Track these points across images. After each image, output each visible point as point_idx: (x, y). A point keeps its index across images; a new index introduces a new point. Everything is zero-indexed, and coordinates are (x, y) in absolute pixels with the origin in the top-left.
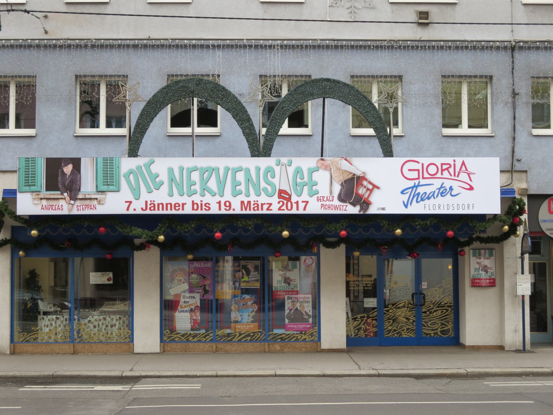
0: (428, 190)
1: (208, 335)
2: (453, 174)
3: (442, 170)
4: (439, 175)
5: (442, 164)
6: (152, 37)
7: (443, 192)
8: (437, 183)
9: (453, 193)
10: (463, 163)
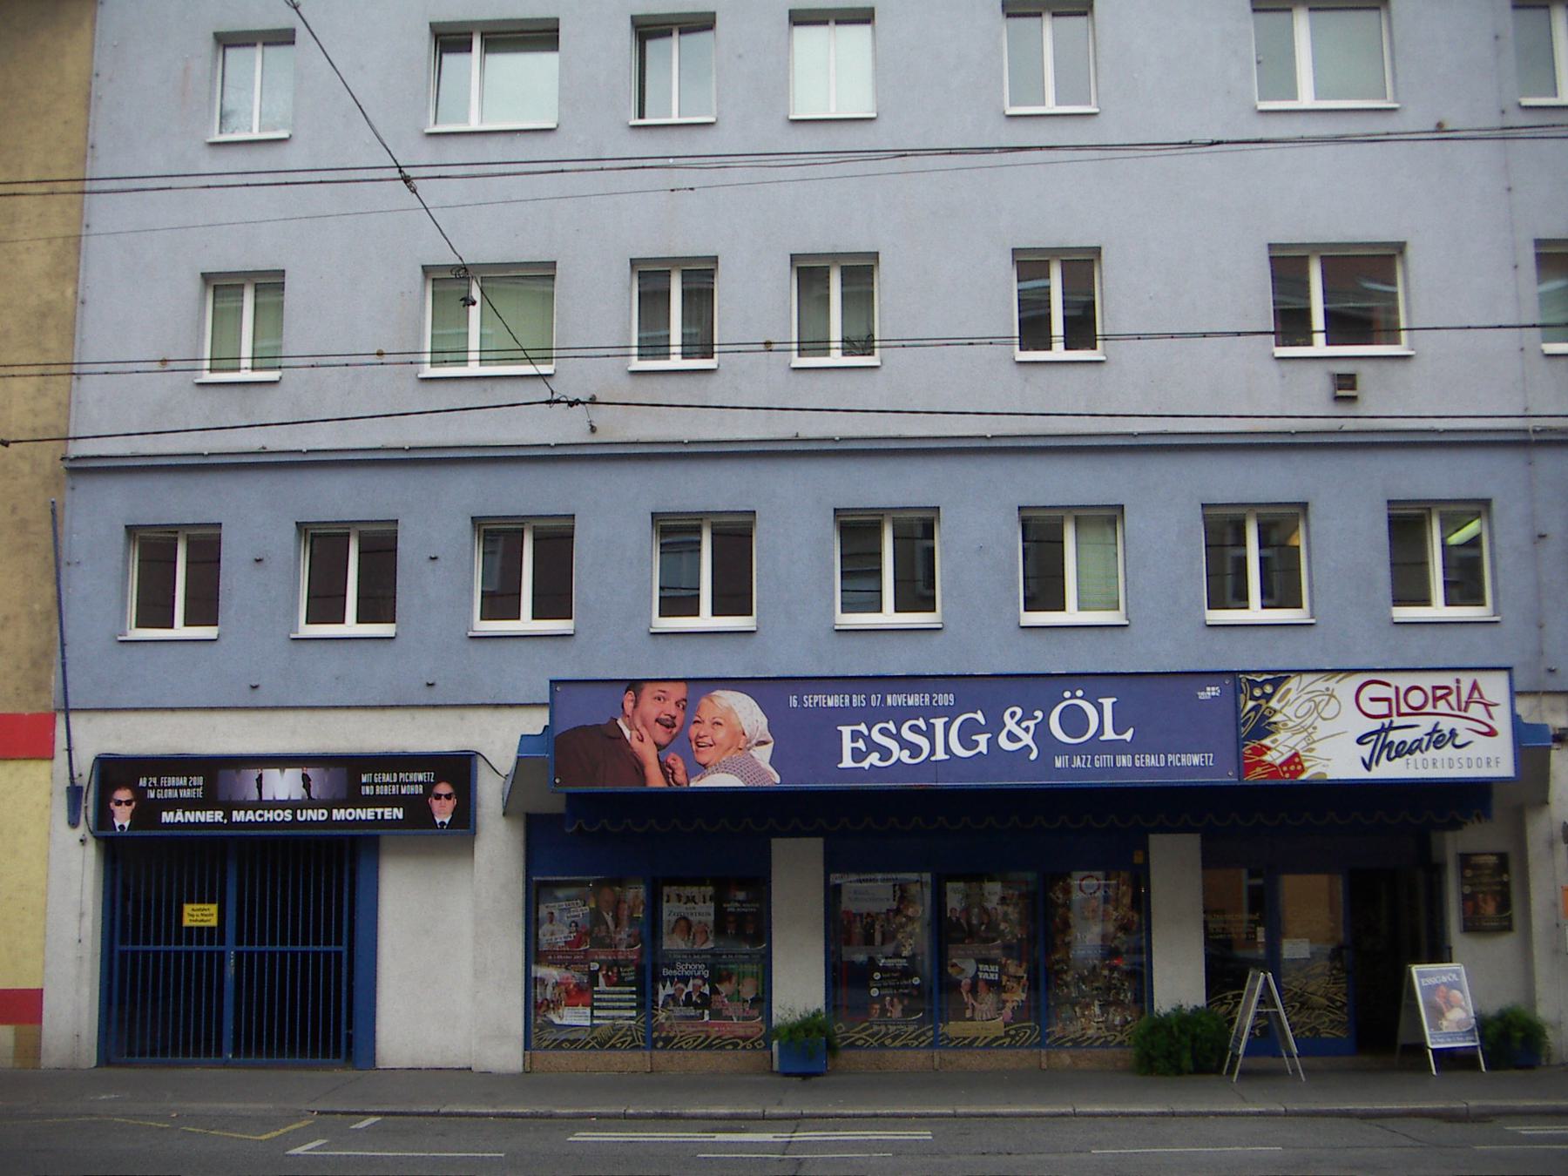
0: (1409, 736)
1: (924, 1033)
2: (1454, 704)
3: (1436, 699)
4: (1429, 709)
5: (1435, 688)
6: (802, 435)
7: (1438, 739)
8: (1426, 724)
9: (1458, 742)
10: (1475, 686)
